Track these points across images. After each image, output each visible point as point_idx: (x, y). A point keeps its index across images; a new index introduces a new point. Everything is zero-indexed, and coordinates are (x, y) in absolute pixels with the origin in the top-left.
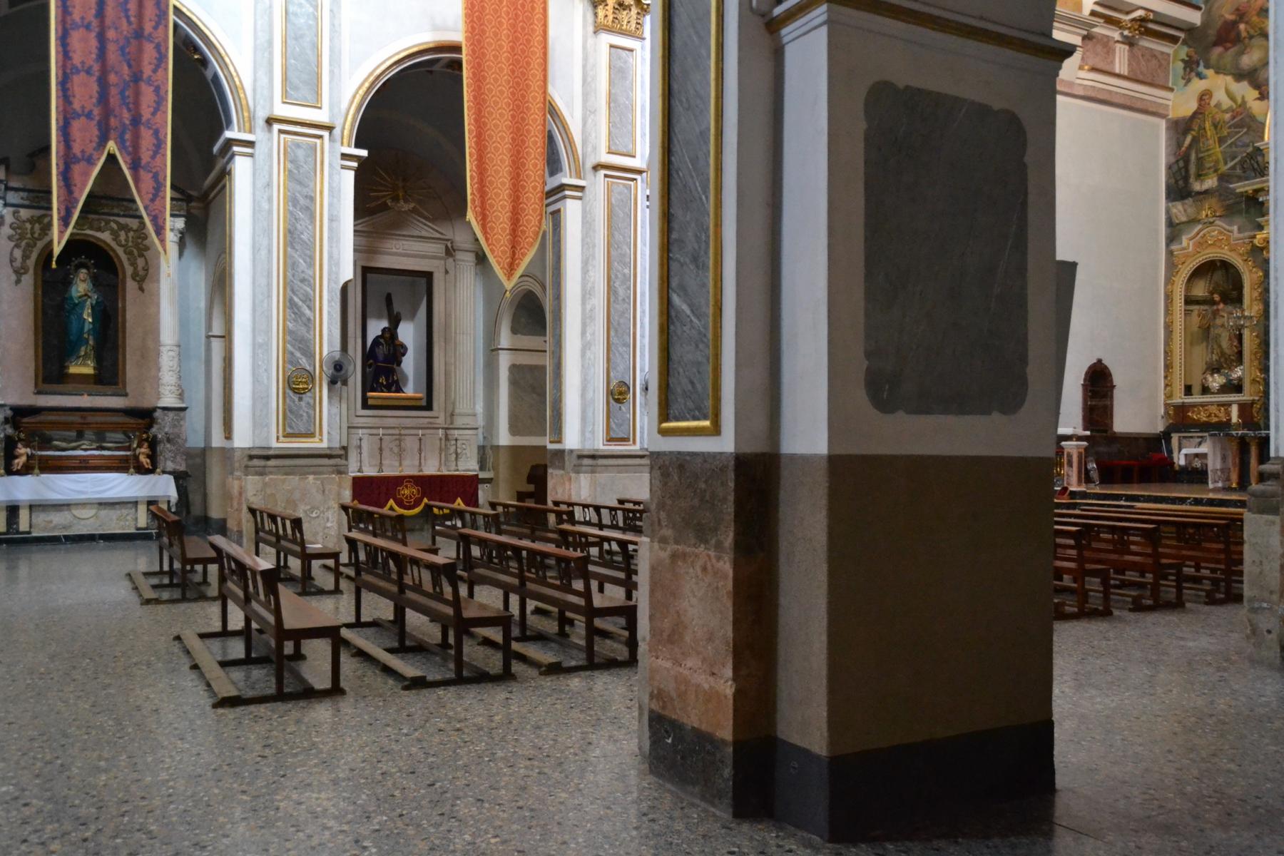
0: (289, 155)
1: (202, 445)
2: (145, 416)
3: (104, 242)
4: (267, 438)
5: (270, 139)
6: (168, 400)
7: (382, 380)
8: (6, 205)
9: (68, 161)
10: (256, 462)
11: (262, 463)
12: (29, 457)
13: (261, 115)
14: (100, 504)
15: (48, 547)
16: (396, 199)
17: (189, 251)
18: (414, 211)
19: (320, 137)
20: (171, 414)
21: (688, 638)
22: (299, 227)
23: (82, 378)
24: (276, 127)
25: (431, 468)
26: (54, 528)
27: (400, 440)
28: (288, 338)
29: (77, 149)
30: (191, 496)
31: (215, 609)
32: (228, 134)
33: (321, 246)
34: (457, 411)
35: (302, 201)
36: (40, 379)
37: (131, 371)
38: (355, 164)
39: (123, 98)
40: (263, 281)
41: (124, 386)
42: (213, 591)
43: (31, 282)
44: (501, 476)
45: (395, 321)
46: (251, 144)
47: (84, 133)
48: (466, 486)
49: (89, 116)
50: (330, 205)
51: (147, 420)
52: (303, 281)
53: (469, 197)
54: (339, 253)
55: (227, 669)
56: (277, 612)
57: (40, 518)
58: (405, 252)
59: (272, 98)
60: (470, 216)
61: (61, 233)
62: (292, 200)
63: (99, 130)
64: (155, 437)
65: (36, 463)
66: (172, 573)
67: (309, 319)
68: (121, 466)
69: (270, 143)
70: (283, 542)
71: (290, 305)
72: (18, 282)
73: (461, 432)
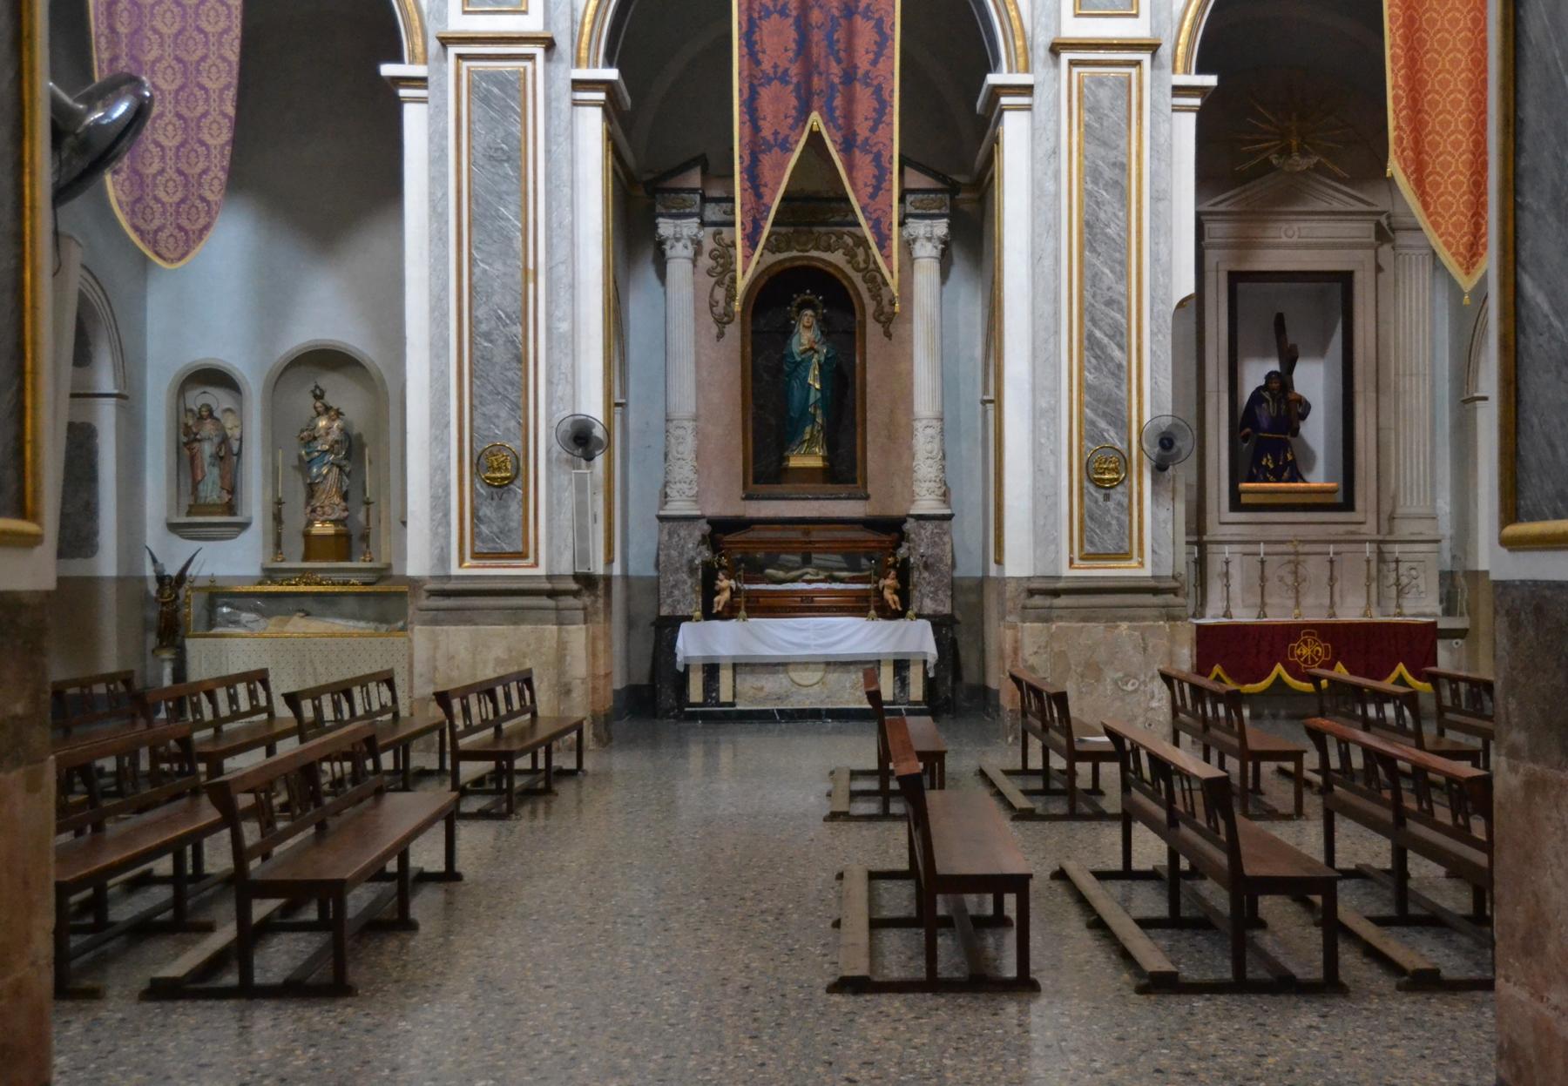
0: (1088, 104)
1: (980, 574)
2: (892, 528)
3: (836, 267)
4: (1056, 561)
5: (1057, 78)
6: (927, 504)
7: (1268, 461)
8: (703, 224)
9: (754, 153)
10: (1038, 600)
11: (1048, 601)
12: (735, 593)
13: (1043, 40)
14: (828, 664)
15: (755, 726)
16: (1285, 152)
17: (958, 270)
18: (1318, 168)
19: (1138, 63)
20: (929, 526)
21: (1551, 947)
22: (1102, 215)
23: (807, 474)
24: (453, 50)
25: (1352, 611)
26: (766, 699)
27: (1297, 564)
28: (1087, 398)
29: (767, 133)
30: (963, 653)
31: (1113, 833)
32: (992, 79)
33: (1139, 243)
34: (1399, 511)
35: (1108, 173)
36: (750, 478)
37: (874, 461)
38: (1197, 102)
39: (831, 43)
40: (1048, 309)
41: (865, 487)
42: (1112, 801)
43: (738, 334)
44: (1483, 627)
45: (1289, 362)
46: (1027, 90)
47: (777, 103)
48: (1415, 643)
49: (784, 78)
50: (1154, 175)
51: (896, 535)
52: (1109, 303)
53: (1392, 134)
54: (1169, 249)
55: (1152, 932)
56: (1233, 848)
57: (748, 683)
58: (1298, 243)
59: (1059, 11)
60: (1394, 167)
61: (747, 258)
62: (1092, 173)
63: (798, 98)
64: (905, 561)
65: (742, 600)
66: (1045, 772)
67: (1120, 366)
68: (857, 606)
69: (1055, 85)
70: (1214, 732)
71: (1090, 344)
72: (721, 335)
73: (1408, 547)
